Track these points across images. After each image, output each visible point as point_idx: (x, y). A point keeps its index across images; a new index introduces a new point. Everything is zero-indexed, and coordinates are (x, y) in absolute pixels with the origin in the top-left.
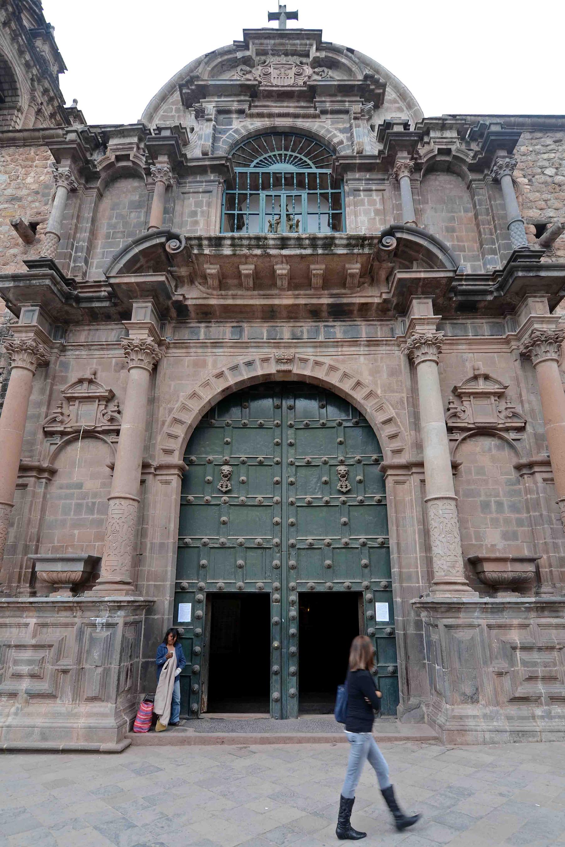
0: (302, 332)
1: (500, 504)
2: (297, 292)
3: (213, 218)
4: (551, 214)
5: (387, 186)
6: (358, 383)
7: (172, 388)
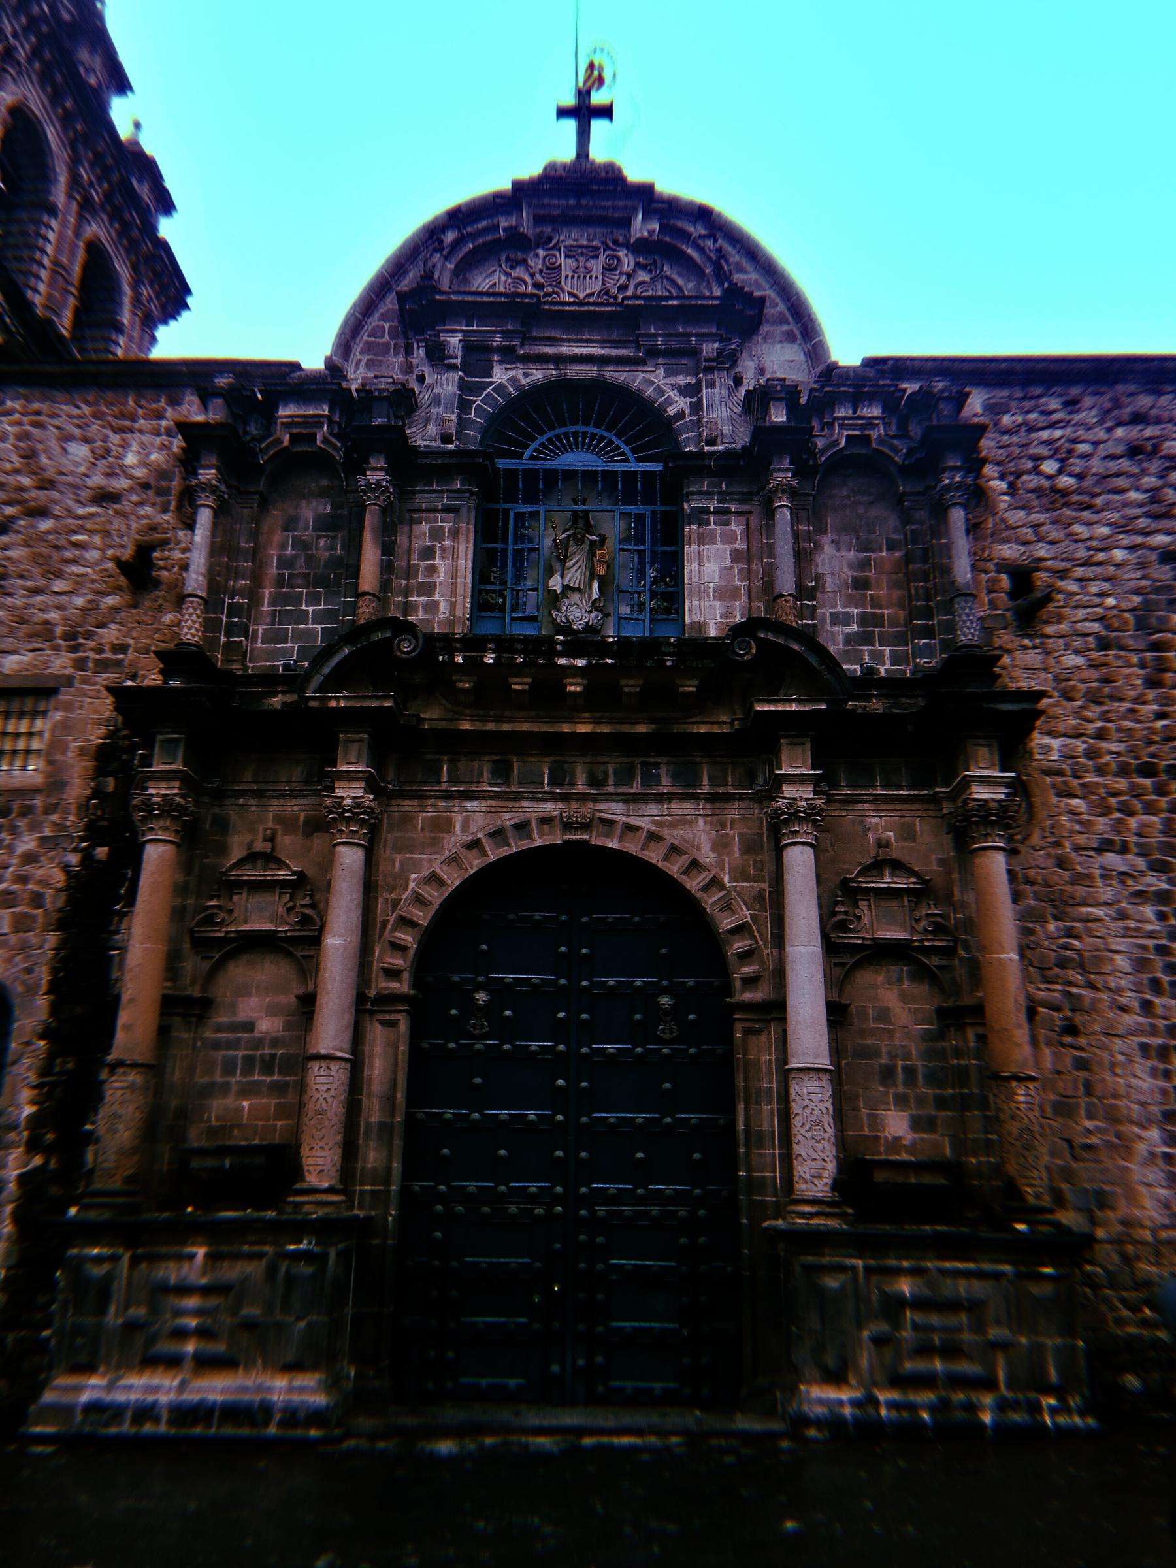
0: (606, 773)
1: (910, 1072)
2: (598, 715)
3: (461, 562)
4: (1042, 553)
5: (755, 507)
6: (695, 865)
7: (397, 865)
